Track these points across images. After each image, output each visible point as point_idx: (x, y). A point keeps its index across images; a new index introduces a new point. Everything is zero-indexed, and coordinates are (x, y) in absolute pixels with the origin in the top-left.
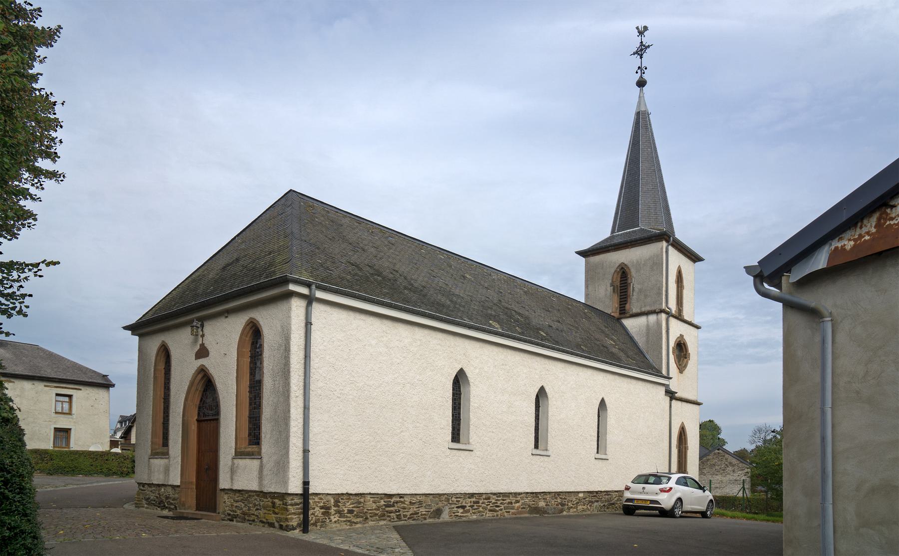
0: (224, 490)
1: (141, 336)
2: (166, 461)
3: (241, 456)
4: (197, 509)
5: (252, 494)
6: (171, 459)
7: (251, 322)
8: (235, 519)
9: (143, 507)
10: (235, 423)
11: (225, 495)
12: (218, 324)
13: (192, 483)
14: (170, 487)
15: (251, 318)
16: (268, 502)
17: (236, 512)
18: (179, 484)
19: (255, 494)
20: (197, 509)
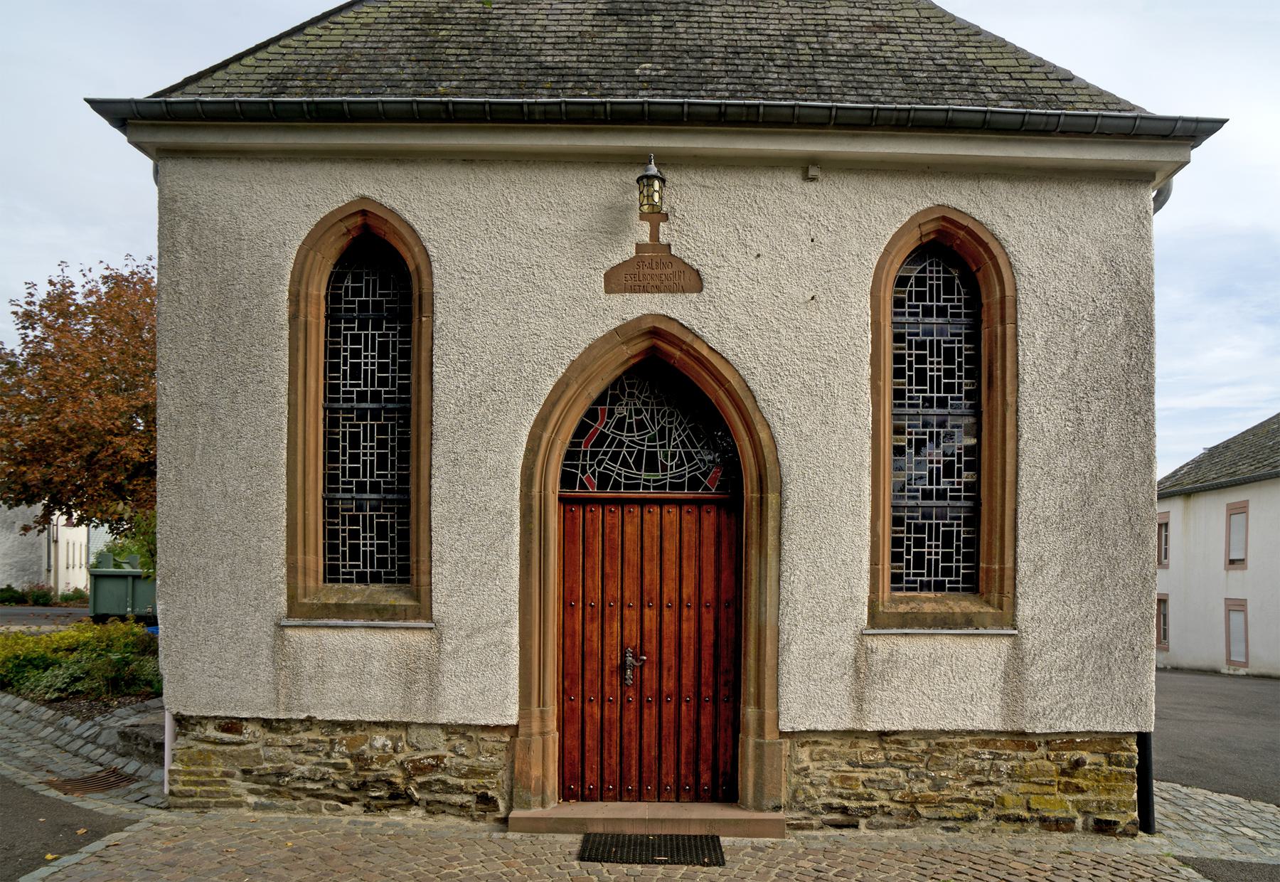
0: (792, 735)
1: (160, 154)
2: (418, 640)
3: (902, 627)
4: (566, 794)
5: (958, 740)
6: (448, 633)
7: (364, 213)
8: (863, 822)
9: (238, 805)
10: (868, 523)
11: (800, 749)
12: (935, 183)
13: (169, 682)
14: (439, 731)
15: (364, 198)
16: (1036, 760)
17: (872, 800)
18: (514, 721)
19: (968, 739)
20: (566, 794)
